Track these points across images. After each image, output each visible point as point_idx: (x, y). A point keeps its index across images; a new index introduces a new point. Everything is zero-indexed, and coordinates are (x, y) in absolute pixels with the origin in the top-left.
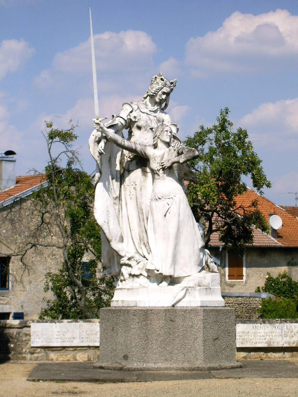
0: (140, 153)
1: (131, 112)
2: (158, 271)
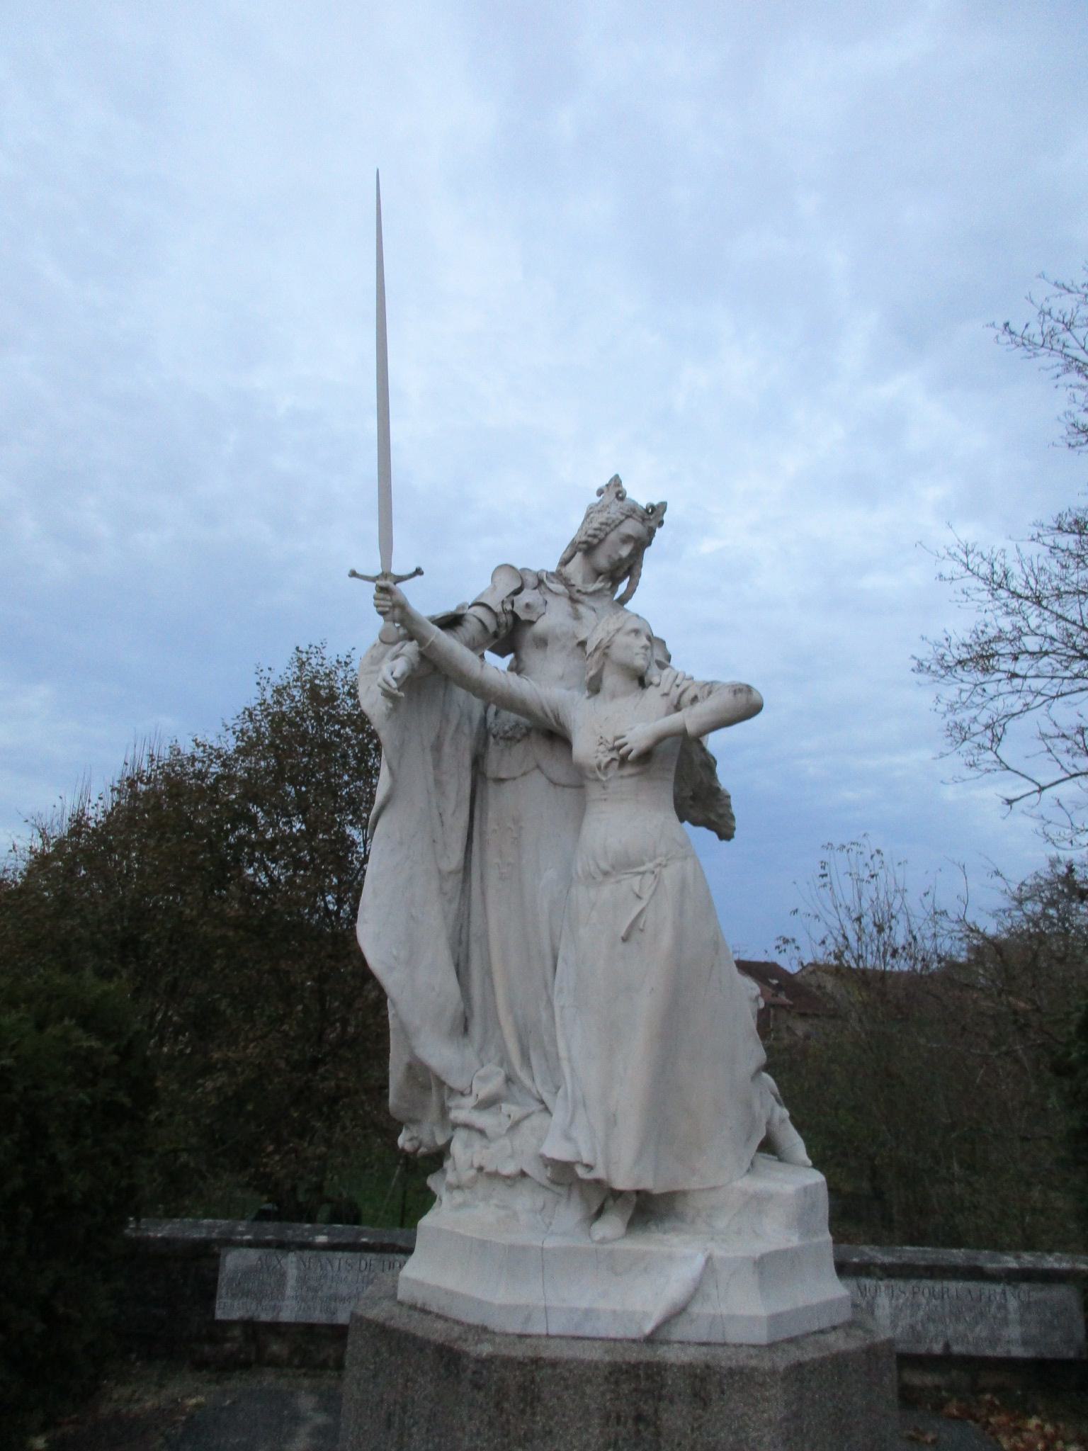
0: (540, 714)
1: (517, 592)
2: (589, 1167)
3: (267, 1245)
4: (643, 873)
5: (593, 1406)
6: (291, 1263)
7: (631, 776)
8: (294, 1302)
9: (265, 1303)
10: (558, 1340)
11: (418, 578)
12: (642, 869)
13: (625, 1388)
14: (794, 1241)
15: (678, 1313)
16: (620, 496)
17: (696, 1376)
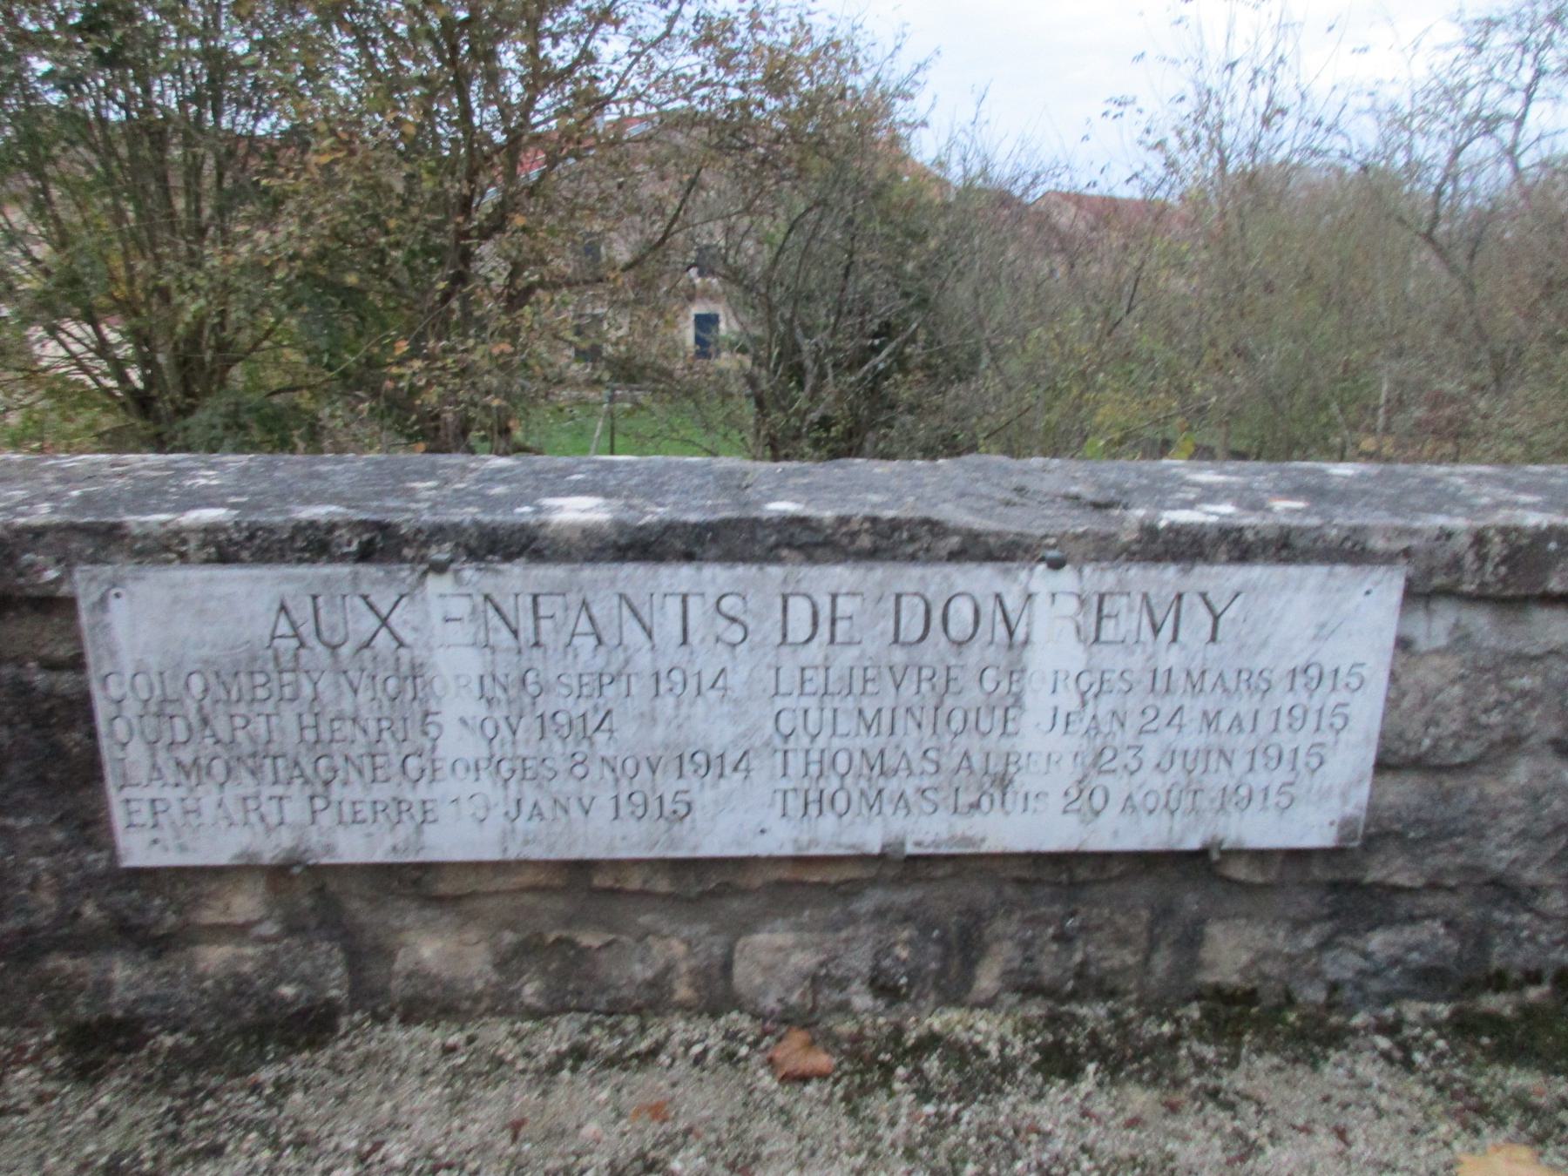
3: (315, 544)
6: (444, 620)
8: (486, 783)
9: (351, 791)
11: (1210, 596)
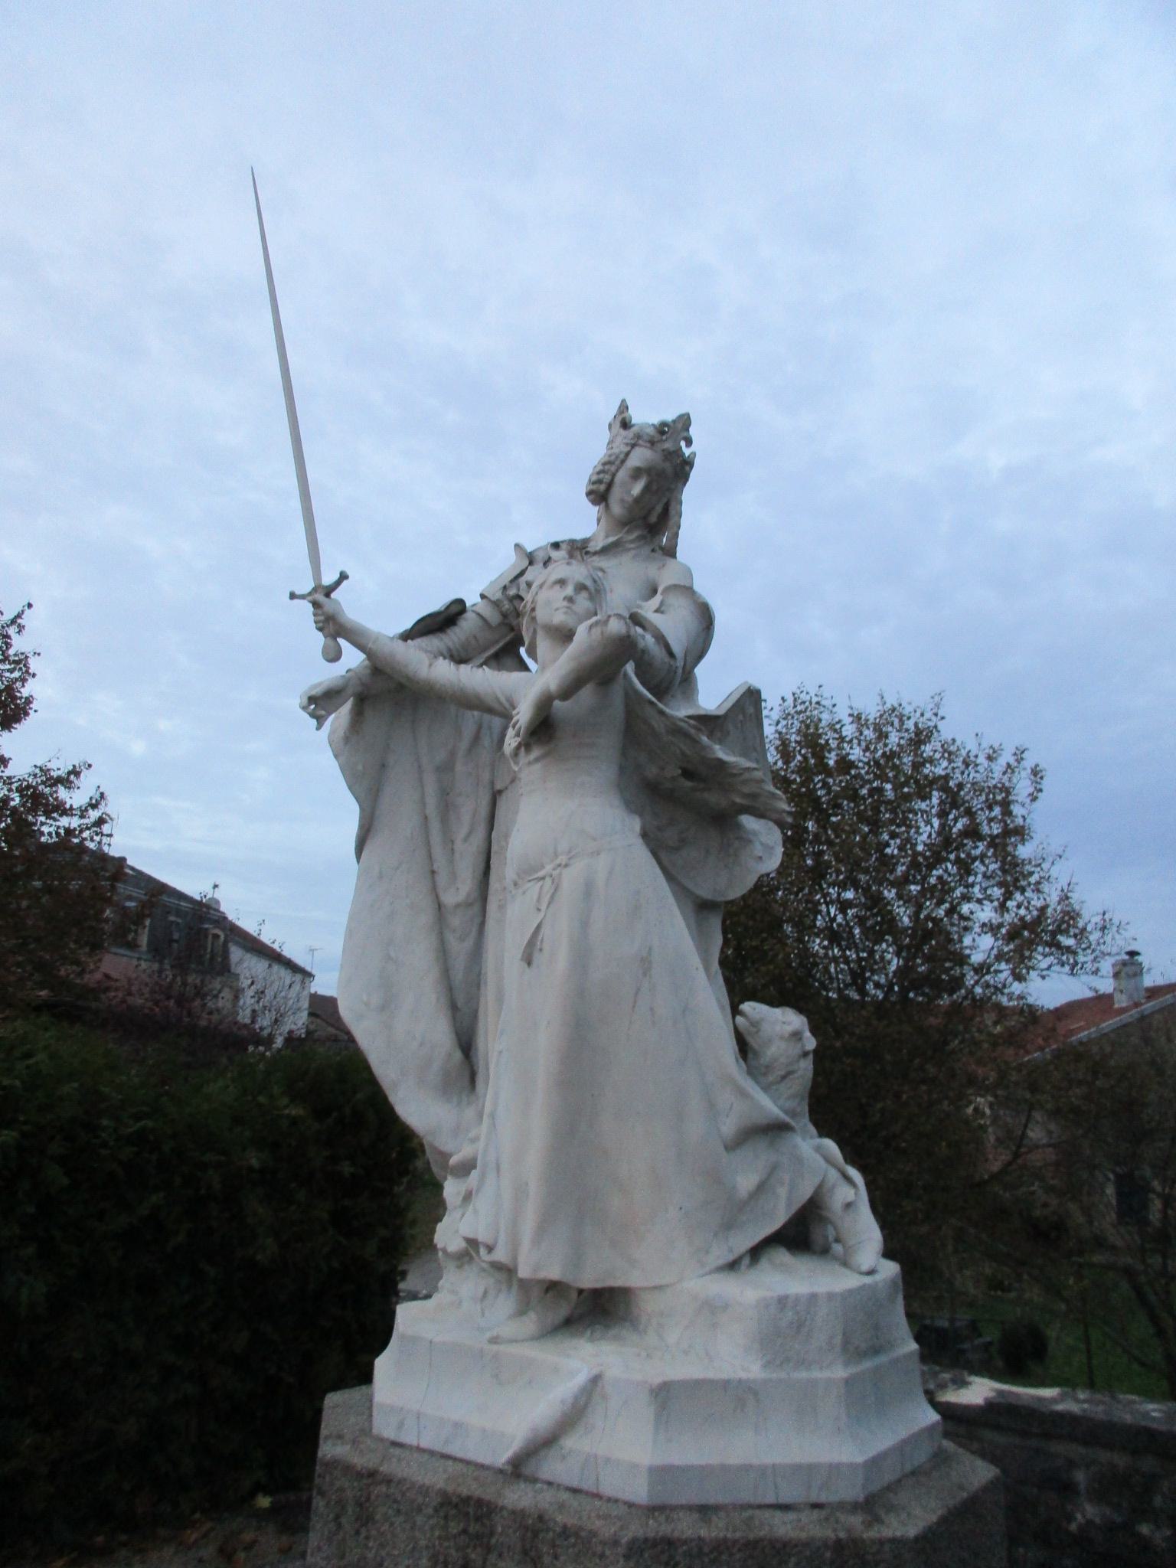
4: (543, 878)
5: (423, 1543)
7: (537, 760)
10: (426, 1456)
11: (345, 582)
12: (541, 874)
13: (454, 1528)
14: (753, 1369)
15: (544, 1443)
16: (625, 425)
17: (526, 1528)
